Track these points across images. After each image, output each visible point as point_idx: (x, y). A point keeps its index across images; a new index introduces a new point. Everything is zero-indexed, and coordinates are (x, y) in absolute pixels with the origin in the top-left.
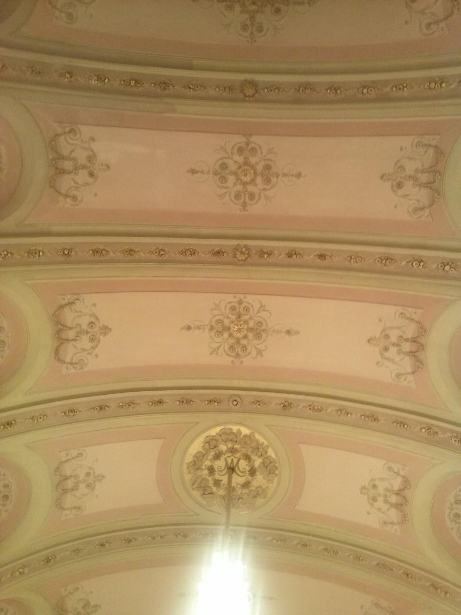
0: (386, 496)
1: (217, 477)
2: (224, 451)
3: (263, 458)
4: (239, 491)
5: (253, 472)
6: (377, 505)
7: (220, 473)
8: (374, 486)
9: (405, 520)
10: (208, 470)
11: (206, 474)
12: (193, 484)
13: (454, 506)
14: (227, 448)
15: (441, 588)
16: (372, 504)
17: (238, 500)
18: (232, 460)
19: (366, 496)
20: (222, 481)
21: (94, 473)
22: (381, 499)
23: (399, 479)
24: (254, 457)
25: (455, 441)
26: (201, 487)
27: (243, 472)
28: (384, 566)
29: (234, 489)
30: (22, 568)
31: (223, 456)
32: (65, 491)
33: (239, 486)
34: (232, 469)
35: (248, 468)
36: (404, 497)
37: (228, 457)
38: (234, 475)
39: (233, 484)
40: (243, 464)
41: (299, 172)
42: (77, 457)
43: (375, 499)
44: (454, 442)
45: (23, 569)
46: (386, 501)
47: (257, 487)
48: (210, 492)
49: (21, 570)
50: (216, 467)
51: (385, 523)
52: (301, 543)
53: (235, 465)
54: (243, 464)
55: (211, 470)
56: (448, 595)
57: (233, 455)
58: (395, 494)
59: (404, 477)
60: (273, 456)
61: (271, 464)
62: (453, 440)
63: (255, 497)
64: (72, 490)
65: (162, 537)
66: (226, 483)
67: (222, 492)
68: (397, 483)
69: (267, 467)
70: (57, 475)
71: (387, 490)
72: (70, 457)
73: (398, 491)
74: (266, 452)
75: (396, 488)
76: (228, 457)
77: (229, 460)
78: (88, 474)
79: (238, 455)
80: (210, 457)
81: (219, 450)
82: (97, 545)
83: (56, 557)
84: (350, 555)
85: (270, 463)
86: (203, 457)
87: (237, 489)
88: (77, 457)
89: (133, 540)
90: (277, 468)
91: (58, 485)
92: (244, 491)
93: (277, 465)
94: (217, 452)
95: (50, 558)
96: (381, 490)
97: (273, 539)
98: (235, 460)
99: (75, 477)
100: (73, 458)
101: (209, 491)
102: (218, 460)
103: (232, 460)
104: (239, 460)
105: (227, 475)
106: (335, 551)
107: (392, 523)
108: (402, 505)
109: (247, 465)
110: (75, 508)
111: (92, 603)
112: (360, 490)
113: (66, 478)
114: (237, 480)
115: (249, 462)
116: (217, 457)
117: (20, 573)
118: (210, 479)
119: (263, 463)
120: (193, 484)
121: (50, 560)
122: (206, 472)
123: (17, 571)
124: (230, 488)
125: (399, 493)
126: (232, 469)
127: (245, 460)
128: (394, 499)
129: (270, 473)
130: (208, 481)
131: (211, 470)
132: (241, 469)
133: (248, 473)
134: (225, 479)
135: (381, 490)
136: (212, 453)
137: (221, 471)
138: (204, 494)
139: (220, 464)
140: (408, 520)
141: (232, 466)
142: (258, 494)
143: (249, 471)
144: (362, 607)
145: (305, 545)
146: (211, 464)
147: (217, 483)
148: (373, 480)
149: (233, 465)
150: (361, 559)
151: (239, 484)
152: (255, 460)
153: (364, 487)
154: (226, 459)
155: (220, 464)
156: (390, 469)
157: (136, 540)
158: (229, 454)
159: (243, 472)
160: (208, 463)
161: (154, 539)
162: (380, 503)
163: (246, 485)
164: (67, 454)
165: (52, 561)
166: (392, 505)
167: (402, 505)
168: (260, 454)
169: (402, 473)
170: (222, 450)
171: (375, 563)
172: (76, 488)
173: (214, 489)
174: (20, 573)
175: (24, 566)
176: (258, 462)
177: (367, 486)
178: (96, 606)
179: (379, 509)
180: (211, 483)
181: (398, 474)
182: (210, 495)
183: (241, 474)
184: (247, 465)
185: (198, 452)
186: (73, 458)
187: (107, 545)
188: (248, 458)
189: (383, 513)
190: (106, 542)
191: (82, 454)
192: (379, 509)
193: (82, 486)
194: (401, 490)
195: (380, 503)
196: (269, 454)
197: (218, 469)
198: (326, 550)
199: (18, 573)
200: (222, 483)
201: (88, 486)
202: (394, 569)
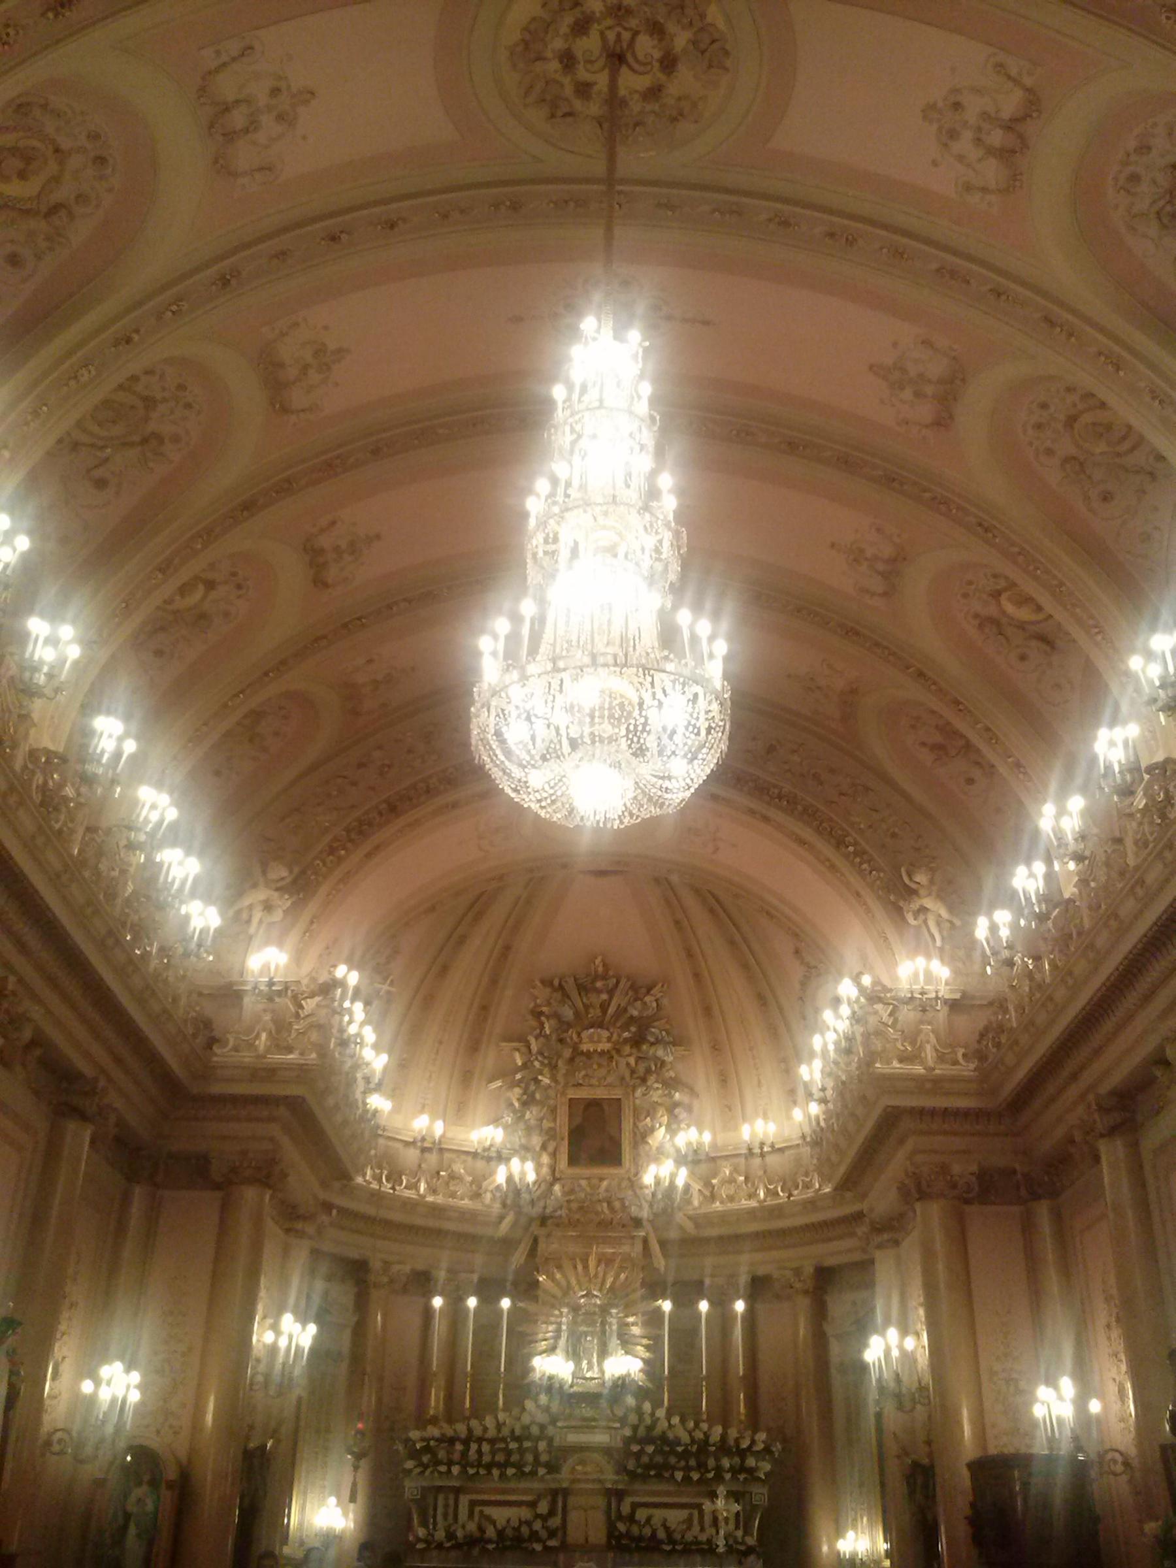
0: (979, 129)
1: (583, 74)
2: (598, 15)
3: (695, 29)
4: (636, 106)
5: (669, 63)
6: (957, 147)
7: (589, 66)
8: (957, 106)
9: (1014, 187)
10: (561, 62)
11: (556, 71)
12: (527, 94)
13: (1133, 158)
14: (605, 6)
15: (1061, 326)
16: (946, 145)
17: (634, 129)
18: (619, 35)
19: (935, 127)
20: (595, 83)
21: (289, 87)
22: (968, 135)
23: (1018, 95)
24: (671, 27)
25: (1168, 18)
26: (544, 100)
27: (645, 64)
28: (953, 274)
29: (623, 103)
30: (174, 303)
31: (596, 25)
32: (230, 136)
33: (636, 96)
34: (617, 58)
35: (657, 54)
36: (1021, 136)
37: (610, 28)
38: (624, 69)
39: (622, 92)
40: (646, 45)
41: (660, 86)
42: (243, 55)
43: (953, 134)
44: (1164, 21)
45: (178, 306)
46: (978, 141)
47: (679, 99)
48: (567, 110)
49: (174, 308)
50: (579, 54)
51: (968, 188)
52: (777, 220)
53: (625, 45)
54: (646, 45)
55: (568, 60)
56: (1073, 339)
57: (619, 25)
58: (1001, 127)
59: (1029, 90)
60: (721, 24)
61: (715, 46)
62: (1163, 17)
63: (674, 120)
64: (246, 131)
65: (462, 211)
66: (605, 89)
67: (595, 108)
68: (1010, 103)
69: (703, 52)
70: (205, 104)
71: (985, 116)
72: (225, 58)
73: (1010, 120)
74: (703, 16)
75: (1007, 112)
76: (610, 28)
77: (611, 36)
78: (275, 92)
79: (633, 23)
80: (564, 29)
81: (583, 13)
82: (323, 239)
83: (239, 273)
84: (881, 248)
85: (713, 42)
86: (547, 33)
87: (631, 103)
88: (243, 55)
89: (400, 222)
90: (727, 53)
91: (211, 126)
92: (648, 108)
93: (728, 47)
94: (579, 16)
95: (228, 277)
96: (971, 115)
97: (714, 211)
98: (626, 36)
99: (248, 101)
100: (234, 59)
101: (565, 109)
102: (585, 38)
103: (619, 35)
104: (636, 34)
105: (607, 71)
106: (850, 237)
107: (984, 190)
108: (1014, 152)
109: (654, 47)
110: (261, 169)
111: (332, 346)
112: (923, 111)
113: (227, 109)
114: (631, 82)
115: (660, 40)
116: (581, 27)
117: (174, 313)
118: (567, 81)
119: (695, 43)
120: (527, 94)
121: (229, 280)
122: (554, 66)
123: (167, 309)
124: (614, 101)
125: (1010, 126)
126: (617, 58)
127: (651, 35)
128: (997, 138)
129: (710, 66)
130: (562, 86)
131: (568, 60)
132: (640, 56)
133: (656, 65)
134: (602, 80)
135: (971, 115)
136: (568, 19)
137: (591, 62)
138: (553, 116)
139: (591, 44)
140: (1021, 187)
141: (618, 50)
142: (681, 115)
143: (661, 61)
144: (895, 345)
145: (785, 223)
146: (567, 46)
147: (584, 90)
148: (956, 91)
149: (621, 47)
150: (905, 256)
151: (636, 91)
152: (675, 35)
153: (932, 107)
154: (602, 33)
155: (591, 44)
156: (1000, 66)
157: (404, 220)
158: (609, 22)
159: (645, 64)
160: (558, 44)
161: (445, 216)
162: (965, 144)
163: (654, 92)
164: (218, 52)
165: (234, 282)
166: (991, 151)
167: (1014, 152)
168: (685, 21)
169: (1028, 81)
170: (593, 12)
171: (934, 266)
172: (253, 125)
173: (578, 104)
174: (174, 313)
175: (179, 299)
176: (681, 40)
177: (940, 104)
178: (340, 351)
179: (960, 158)
180: (569, 90)
181: (1016, 82)
182: (569, 119)
183: (642, 69)
184: (654, 47)
185: (534, 19)
186: (234, 59)
187: (344, 237)
188: (657, 29)
189: (969, 165)
190: (342, 232)
191: (251, 48)
192: (960, 158)
193: (266, 120)
194: (1017, 120)
195: (965, 144)
196: (709, 19)
197: (583, 55)
198: (832, 235)
199: (170, 314)
200: (596, 88)
201: (280, 118)
202: (972, 281)
